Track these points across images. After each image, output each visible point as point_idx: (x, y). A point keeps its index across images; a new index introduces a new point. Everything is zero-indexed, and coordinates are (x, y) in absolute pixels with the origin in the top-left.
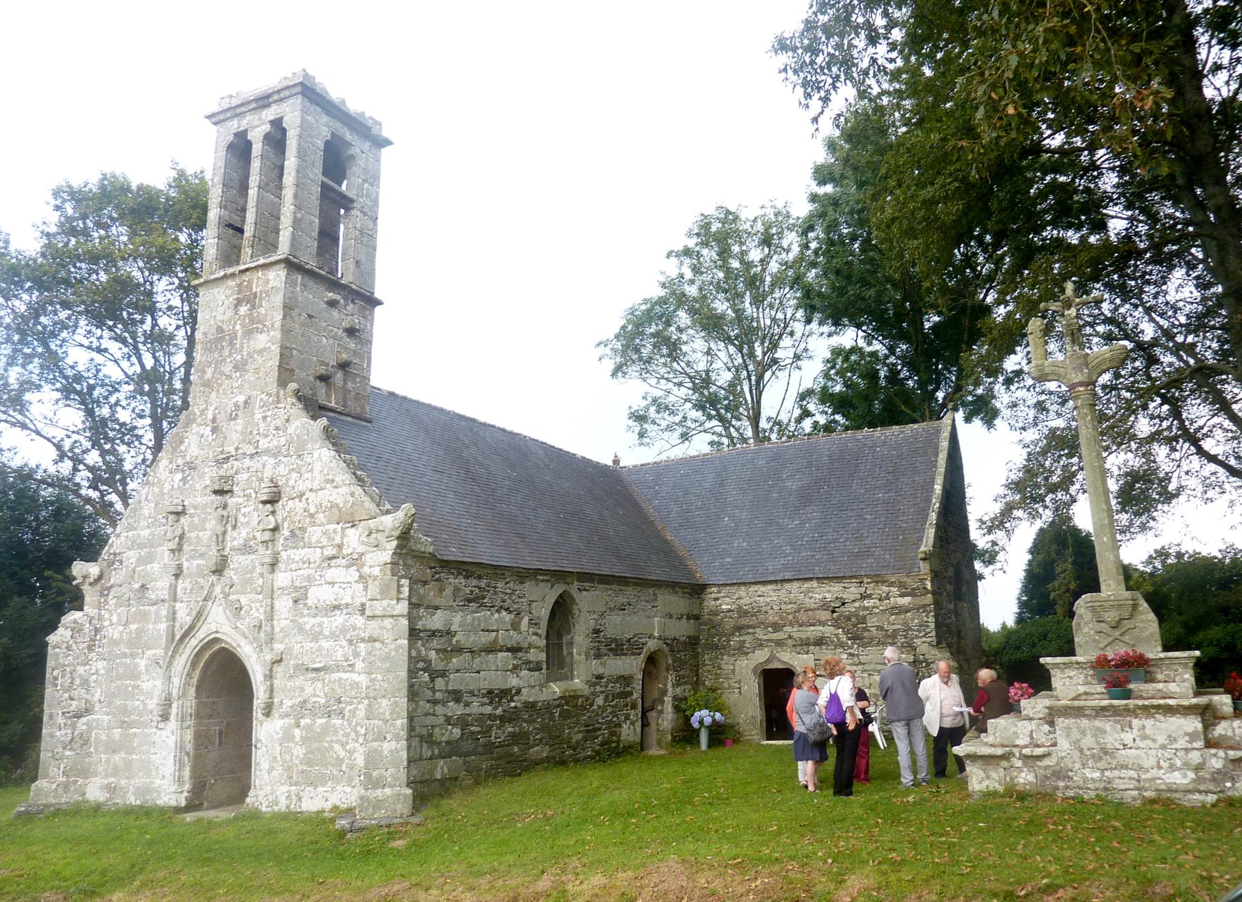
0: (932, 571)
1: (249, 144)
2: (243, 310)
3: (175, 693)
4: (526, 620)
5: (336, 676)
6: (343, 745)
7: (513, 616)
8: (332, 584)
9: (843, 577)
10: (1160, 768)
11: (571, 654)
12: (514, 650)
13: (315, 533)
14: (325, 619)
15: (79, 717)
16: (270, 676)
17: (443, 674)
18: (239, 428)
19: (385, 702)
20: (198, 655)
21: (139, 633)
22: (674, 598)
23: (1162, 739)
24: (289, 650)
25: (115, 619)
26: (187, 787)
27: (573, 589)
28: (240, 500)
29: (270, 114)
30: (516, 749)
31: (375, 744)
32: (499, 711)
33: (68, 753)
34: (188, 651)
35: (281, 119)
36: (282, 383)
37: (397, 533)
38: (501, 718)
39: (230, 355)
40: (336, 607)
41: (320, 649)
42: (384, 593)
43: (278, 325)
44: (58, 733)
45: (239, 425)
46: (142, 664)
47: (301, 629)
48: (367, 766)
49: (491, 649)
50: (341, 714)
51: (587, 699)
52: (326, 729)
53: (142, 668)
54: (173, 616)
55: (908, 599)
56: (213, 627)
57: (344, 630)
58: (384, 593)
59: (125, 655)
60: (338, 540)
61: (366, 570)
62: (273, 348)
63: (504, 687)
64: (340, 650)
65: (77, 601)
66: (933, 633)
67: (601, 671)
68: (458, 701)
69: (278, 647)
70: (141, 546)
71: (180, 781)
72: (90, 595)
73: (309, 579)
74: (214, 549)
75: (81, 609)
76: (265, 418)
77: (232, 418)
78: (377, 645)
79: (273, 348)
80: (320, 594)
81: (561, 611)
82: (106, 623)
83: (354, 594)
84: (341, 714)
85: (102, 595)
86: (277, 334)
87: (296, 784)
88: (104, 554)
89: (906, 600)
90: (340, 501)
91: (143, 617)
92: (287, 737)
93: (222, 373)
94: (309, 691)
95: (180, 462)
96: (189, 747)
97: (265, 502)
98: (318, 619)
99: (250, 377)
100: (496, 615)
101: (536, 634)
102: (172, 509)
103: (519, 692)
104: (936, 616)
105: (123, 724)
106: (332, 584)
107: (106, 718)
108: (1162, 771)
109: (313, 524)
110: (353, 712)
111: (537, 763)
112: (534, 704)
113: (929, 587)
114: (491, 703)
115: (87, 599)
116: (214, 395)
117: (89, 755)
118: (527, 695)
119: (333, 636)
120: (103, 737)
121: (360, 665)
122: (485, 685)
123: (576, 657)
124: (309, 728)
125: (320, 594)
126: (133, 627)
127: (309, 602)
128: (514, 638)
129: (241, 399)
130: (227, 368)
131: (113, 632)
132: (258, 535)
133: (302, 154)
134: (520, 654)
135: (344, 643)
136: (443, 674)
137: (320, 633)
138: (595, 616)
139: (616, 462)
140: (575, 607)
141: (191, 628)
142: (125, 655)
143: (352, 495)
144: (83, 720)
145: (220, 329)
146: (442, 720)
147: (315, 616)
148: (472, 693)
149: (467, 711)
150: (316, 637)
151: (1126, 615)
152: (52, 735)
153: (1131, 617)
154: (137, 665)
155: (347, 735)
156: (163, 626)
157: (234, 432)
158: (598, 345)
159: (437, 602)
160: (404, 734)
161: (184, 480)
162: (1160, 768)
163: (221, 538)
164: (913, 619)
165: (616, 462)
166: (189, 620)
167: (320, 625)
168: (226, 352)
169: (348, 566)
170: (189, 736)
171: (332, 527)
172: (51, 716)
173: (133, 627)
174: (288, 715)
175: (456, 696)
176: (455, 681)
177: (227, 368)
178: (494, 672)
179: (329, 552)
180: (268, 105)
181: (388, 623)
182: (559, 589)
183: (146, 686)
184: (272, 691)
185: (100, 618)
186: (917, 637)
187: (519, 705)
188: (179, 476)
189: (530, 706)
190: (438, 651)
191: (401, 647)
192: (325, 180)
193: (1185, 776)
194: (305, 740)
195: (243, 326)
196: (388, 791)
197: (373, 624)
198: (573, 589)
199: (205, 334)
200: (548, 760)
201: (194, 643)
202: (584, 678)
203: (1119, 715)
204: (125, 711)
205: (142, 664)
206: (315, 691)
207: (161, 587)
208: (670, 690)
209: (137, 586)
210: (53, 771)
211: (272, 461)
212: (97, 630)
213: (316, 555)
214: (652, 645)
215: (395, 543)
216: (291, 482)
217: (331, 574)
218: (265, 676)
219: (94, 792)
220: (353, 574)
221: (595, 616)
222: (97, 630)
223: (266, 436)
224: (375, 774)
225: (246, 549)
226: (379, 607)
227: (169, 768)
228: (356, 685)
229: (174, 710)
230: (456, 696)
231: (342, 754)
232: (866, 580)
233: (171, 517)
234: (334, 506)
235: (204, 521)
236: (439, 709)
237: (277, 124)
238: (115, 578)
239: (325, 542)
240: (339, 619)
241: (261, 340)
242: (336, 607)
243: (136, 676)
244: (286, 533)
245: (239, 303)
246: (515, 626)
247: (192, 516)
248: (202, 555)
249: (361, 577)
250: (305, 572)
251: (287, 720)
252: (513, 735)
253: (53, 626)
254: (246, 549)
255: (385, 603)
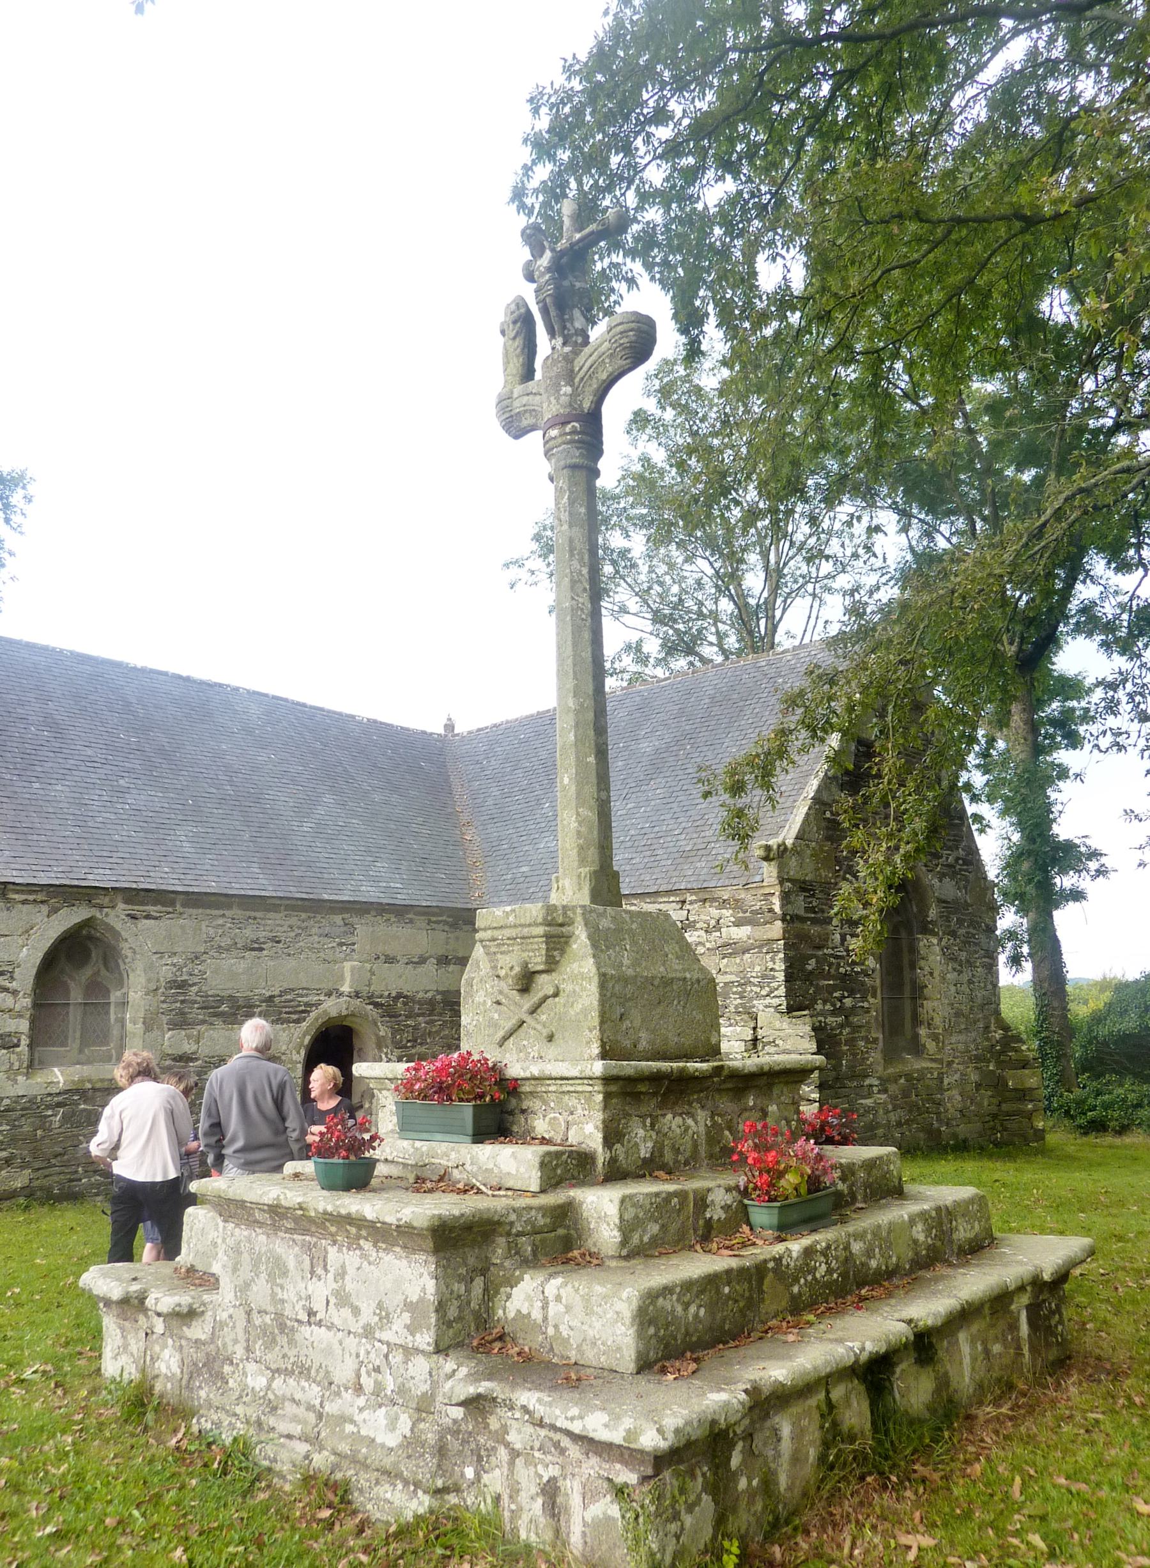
9: (657, 893)
11: (122, 1022)
22: (408, 931)
27: (116, 917)
66: (782, 991)
67: (188, 1047)
89: (742, 933)
104: (787, 959)
108: (361, 1401)
113: (777, 908)
123: (129, 1026)
139: (449, 727)
140: (123, 945)
151: (537, 961)
153: (552, 965)
158: (507, 565)
164: (752, 965)
165: (449, 727)
186: (758, 996)
200: (29, 1192)
203: (305, 1232)
214: (332, 1007)
232: (690, 898)
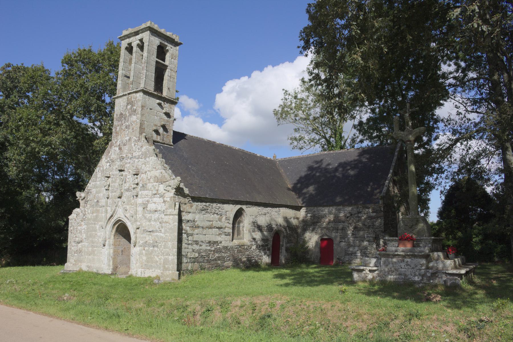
0: (384, 203)
1: (132, 48)
2: (129, 107)
3: (107, 236)
4: (224, 218)
5: (156, 234)
6: (158, 256)
7: (219, 216)
8: (155, 203)
10: (411, 275)
11: (243, 230)
12: (219, 228)
13: (149, 186)
14: (153, 215)
15: (79, 243)
16: (135, 233)
17: (192, 235)
18: (127, 148)
19: (170, 243)
20: (114, 225)
21: (97, 216)
23: (413, 266)
24: (141, 224)
25: (89, 212)
26: (111, 267)
28: (127, 173)
29: (139, 37)
30: (219, 262)
31: (167, 257)
32: (213, 249)
33: (76, 255)
34: (111, 223)
35: (142, 39)
36: (141, 133)
37: (175, 187)
38: (214, 251)
39: (125, 122)
40: (156, 211)
41: (151, 225)
42: (170, 207)
43: (140, 113)
44: (72, 248)
45: (127, 147)
46: (98, 227)
47: (145, 218)
48: (164, 262)
49: (210, 228)
50: (157, 246)
51: (249, 246)
52: (152, 251)
53: (98, 228)
54: (106, 211)
55: (375, 214)
56: (119, 216)
57: (158, 219)
58: (170, 207)
59: (92, 224)
60: (157, 188)
61: (165, 199)
62: (138, 121)
63: (215, 240)
64: (157, 225)
65: (78, 205)
66: (383, 227)
68: (197, 244)
69: (138, 223)
70: (97, 187)
71: (109, 265)
72: (82, 203)
73: (148, 201)
74: (119, 189)
75: (79, 207)
76: (135, 145)
77: (124, 145)
78: (168, 224)
79: (138, 121)
80: (151, 206)
81: (239, 214)
82: (87, 213)
83: (161, 207)
84: (157, 246)
85: (85, 203)
86: (139, 116)
87: (144, 268)
88: (86, 190)
90: (158, 175)
91: (98, 211)
92: (141, 254)
93: (122, 129)
94: (147, 239)
95: (109, 159)
96: (112, 255)
97: (134, 175)
98: (150, 215)
99: (131, 130)
100: (212, 216)
101: (228, 223)
102: (106, 175)
103: (221, 243)
105: (93, 246)
106: (155, 203)
107: (87, 244)
109: (149, 183)
110: (161, 246)
111: (227, 267)
112: (227, 247)
113: (382, 209)
114: (210, 246)
115: (81, 204)
116: (119, 137)
117: (82, 255)
118: (224, 244)
119: (155, 220)
120: (86, 250)
121: (163, 231)
122: (208, 239)
123: (245, 231)
124: (147, 251)
125: (151, 206)
126: (95, 214)
127: (148, 209)
128: (219, 224)
129: (127, 138)
130: (124, 127)
131: (89, 216)
132: (132, 185)
133: (149, 52)
134: (221, 230)
135: (158, 223)
136: (192, 235)
137: (151, 219)
138: (253, 217)
141: (112, 216)
142: (92, 224)
143: (161, 173)
144: (80, 244)
145: (121, 114)
146: (191, 250)
147: (150, 214)
148: (202, 242)
149: (201, 248)
150: (150, 221)
152: (71, 249)
154: (96, 227)
155: (159, 253)
156: (103, 215)
157: (125, 149)
159: (190, 210)
160: (176, 254)
161: (110, 165)
162: (411, 275)
163: (121, 185)
166: (111, 213)
167: (151, 217)
168: (123, 122)
169: (160, 197)
170: (112, 251)
171: (155, 184)
172: (70, 242)
173: (95, 214)
174: (141, 246)
175: (197, 243)
176: (196, 237)
177: (124, 127)
178: (212, 235)
179: (155, 192)
180: (138, 34)
181: (171, 217)
182: (238, 207)
183: (99, 234)
184: (136, 238)
185: (85, 211)
187: (221, 247)
188: (108, 164)
189: (226, 248)
190: (190, 227)
191: (175, 225)
192: (157, 60)
193: (418, 278)
194: (146, 254)
195: (129, 112)
196: (170, 272)
197: (166, 217)
198: (244, 207)
199: (117, 115)
201: (113, 221)
202: (248, 239)
204: (93, 242)
205: (98, 227)
206: (149, 238)
207: (103, 202)
208: (285, 245)
209: (96, 201)
210: (71, 261)
211: (137, 160)
212: (84, 215)
213: (150, 193)
215: (174, 190)
216: (143, 168)
217: (155, 199)
218: (134, 233)
219: (84, 268)
220: (161, 200)
221: (253, 217)
222: (84, 215)
223: (135, 152)
224: (166, 266)
225: (128, 190)
226: (169, 211)
227: (106, 261)
228: (162, 237)
229: (107, 243)
230: (197, 243)
231: (158, 259)
233: (106, 178)
234: (155, 177)
235: (116, 180)
236: (190, 247)
237: (141, 40)
238: (90, 197)
239: (153, 189)
240: (156, 215)
241: (134, 118)
242: (156, 211)
243: (95, 231)
244: (141, 185)
245: (128, 104)
246: (220, 220)
247: (112, 178)
248: (115, 192)
249: (164, 201)
250: (147, 199)
251: (141, 248)
252: (219, 257)
253: (70, 213)
254: (128, 190)
255: (170, 210)
